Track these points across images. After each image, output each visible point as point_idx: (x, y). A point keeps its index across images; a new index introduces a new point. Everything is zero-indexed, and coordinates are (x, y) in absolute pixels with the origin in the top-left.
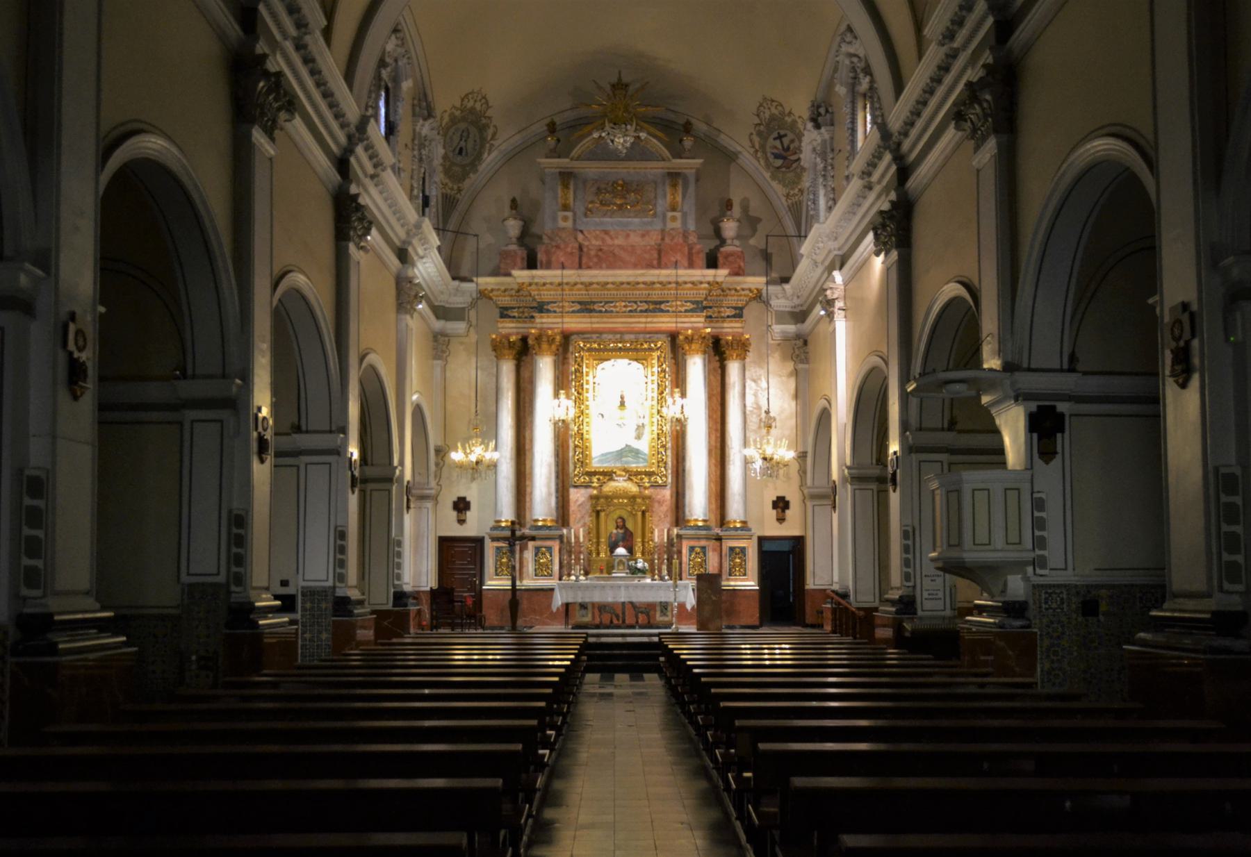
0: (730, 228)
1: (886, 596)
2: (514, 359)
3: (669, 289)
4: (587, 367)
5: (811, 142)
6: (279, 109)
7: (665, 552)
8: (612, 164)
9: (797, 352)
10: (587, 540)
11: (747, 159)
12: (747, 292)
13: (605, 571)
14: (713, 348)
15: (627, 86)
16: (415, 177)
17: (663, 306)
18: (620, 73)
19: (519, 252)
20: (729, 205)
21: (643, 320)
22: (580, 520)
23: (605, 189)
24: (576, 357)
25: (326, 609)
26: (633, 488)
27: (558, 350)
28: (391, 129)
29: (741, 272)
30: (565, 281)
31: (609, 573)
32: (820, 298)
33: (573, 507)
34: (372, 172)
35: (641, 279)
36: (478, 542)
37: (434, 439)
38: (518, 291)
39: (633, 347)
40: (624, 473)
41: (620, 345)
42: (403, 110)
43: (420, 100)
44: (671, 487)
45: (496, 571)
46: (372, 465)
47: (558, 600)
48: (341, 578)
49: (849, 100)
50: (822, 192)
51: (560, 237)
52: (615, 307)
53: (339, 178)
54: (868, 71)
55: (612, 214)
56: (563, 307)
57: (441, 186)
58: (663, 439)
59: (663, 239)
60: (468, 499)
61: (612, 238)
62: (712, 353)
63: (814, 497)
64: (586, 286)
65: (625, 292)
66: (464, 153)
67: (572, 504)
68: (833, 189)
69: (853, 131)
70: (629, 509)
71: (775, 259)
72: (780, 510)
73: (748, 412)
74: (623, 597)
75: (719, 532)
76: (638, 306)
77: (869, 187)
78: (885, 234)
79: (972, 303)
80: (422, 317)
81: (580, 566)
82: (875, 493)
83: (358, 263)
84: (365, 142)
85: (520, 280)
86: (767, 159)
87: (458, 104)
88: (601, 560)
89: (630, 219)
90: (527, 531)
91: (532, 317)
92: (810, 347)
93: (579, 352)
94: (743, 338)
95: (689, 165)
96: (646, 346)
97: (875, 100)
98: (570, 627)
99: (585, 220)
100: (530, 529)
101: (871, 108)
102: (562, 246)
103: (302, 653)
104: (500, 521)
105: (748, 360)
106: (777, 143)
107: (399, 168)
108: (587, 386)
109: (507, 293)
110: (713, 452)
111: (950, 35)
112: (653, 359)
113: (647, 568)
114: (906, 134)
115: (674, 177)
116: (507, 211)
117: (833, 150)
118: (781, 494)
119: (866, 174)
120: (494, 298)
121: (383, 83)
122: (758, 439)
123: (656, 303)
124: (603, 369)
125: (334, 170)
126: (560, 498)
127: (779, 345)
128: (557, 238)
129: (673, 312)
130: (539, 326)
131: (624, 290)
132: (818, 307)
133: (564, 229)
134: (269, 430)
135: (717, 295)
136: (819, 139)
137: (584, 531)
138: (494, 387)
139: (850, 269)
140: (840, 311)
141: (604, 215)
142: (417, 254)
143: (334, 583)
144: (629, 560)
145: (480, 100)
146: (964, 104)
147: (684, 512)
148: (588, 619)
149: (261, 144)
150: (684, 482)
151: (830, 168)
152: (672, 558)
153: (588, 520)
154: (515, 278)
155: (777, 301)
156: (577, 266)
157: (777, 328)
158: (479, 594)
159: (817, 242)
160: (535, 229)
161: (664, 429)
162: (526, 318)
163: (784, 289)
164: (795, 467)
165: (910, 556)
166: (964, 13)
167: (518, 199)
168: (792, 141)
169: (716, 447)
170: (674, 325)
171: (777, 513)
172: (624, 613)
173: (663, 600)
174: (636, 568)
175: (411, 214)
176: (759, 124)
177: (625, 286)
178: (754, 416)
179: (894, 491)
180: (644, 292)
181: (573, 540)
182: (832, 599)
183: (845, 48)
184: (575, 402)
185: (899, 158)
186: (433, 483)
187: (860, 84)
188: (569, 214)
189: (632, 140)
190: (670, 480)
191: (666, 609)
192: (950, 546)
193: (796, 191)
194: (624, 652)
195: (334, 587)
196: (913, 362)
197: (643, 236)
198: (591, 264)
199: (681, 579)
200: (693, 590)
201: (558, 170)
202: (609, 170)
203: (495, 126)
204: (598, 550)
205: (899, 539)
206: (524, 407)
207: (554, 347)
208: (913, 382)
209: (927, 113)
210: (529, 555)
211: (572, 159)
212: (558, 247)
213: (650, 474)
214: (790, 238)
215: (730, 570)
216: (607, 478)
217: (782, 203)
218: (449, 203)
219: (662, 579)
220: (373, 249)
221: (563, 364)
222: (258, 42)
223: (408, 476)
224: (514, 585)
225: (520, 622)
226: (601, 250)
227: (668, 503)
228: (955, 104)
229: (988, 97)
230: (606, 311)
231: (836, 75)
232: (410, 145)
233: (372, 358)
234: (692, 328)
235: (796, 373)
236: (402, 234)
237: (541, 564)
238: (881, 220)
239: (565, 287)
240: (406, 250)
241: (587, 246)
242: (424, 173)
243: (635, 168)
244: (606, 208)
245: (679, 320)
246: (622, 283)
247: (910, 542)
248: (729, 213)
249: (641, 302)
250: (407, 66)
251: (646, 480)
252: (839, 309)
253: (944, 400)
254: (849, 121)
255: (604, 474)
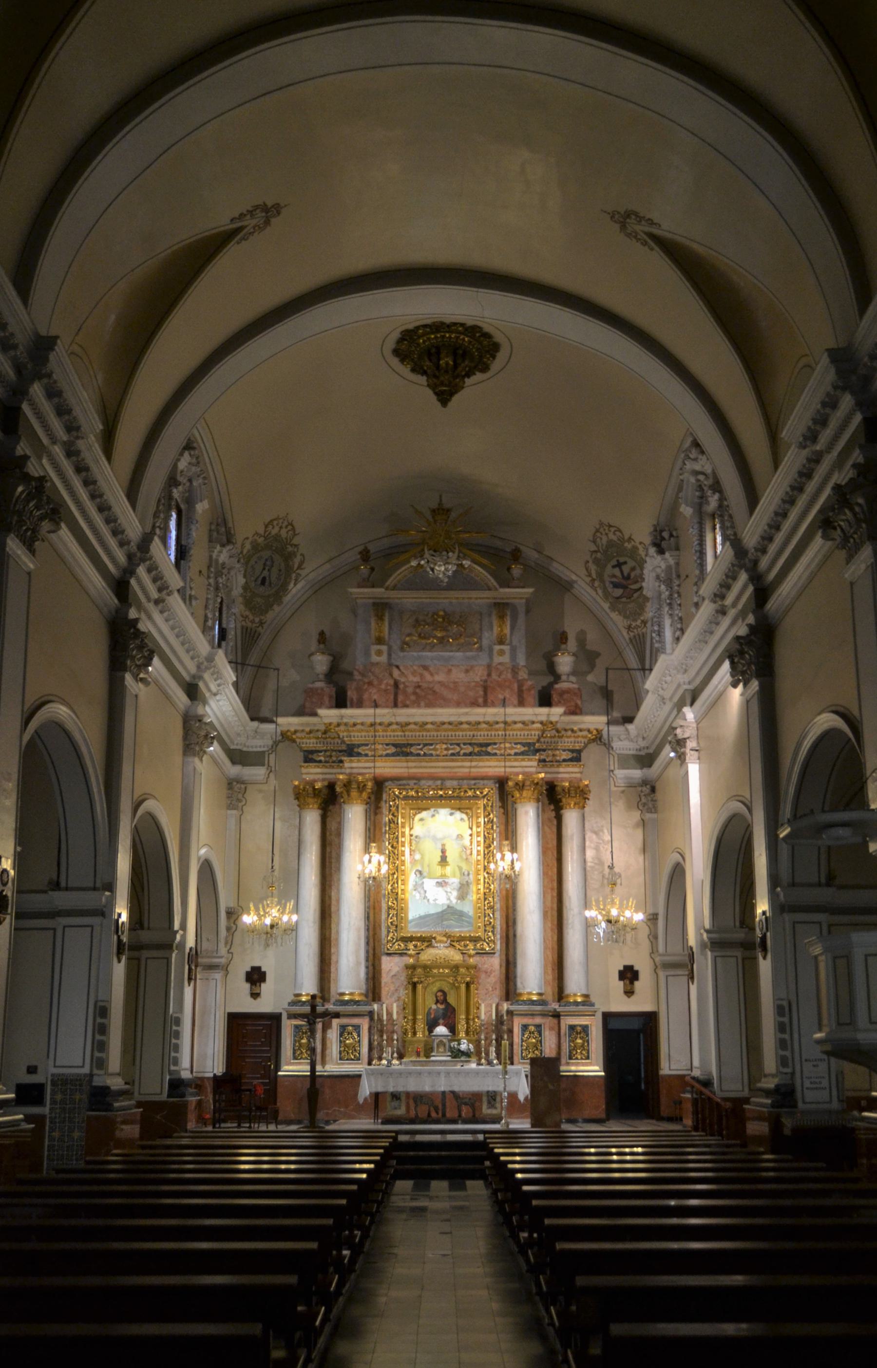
0: (565, 662)
1: (759, 1085)
2: (319, 808)
3: (497, 730)
4: (402, 817)
5: (653, 570)
6: (42, 518)
7: (493, 1031)
8: (434, 594)
9: (644, 800)
10: (401, 1016)
11: (584, 589)
12: (585, 733)
13: (422, 1054)
14: (547, 796)
15: (448, 510)
16: (210, 607)
17: (489, 749)
18: (441, 496)
19: (327, 690)
20: (563, 638)
21: (468, 764)
22: (393, 994)
23: (424, 621)
24: (390, 806)
25: (80, 1100)
26: (456, 957)
27: (369, 798)
28: (182, 552)
29: (578, 711)
30: (378, 720)
31: (428, 1056)
32: (669, 738)
33: (385, 979)
34: (156, 597)
35: (464, 719)
36: (274, 1019)
37: (225, 900)
38: (325, 732)
39: (455, 794)
40: (445, 939)
41: (441, 793)
42: (198, 534)
43: (218, 525)
44: (500, 955)
45: (294, 1053)
46: (149, 929)
47: (366, 1090)
48: (100, 1064)
49: (695, 520)
50: (667, 622)
51: (373, 673)
52: (435, 749)
53: (116, 601)
54: (717, 487)
55: (432, 647)
56: (375, 750)
57: (241, 619)
58: (491, 899)
59: (489, 675)
60: (263, 969)
61: (432, 675)
62: (546, 801)
63: (667, 966)
64: (402, 726)
65: (446, 734)
66: (267, 584)
67: (384, 975)
68: (681, 619)
69: (702, 554)
70: (451, 980)
71: (616, 697)
72: (628, 982)
73: (588, 869)
74: (442, 1085)
75: (557, 1007)
76: (461, 749)
77: (723, 612)
78: (743, 662)
79: (851, 735)
80: (214, 760)
81: (392, 1047)
82: (740, 961)
83: (136, 696)
84: (148, 563)
85: (327, 721)
86: (605, 590)
87: (261, 531)
88: (419, 1041)
89: (451, 654)
90: (330, 1007)
91: (341, 761)
92: (659, 795)
93: (394, 800)
94: (581, 785)
95: (519, 594)
96: (470, 793)
97: (726, 518)
98: (380, 1121)
99: (402, 654)
100: (334, 1004)
101: (723, 528)
102: (375, 682)
103: (49, 1156)
104: (300, 995)
105: (587, 809)
106: (617, 572)
107: (190, 596)
108: (403, 839)
109: (311, 735)
110: (549, 914)
111: (811, 437)
112: (479, 808)
113: (472, 1050)
114: (764, 551)
115: (501, 608)
116: (314, 645)
117: (679, 576)
118: (628, 963)
119: (719, 596)
120: (298, 741)
121: (173, 503)
122: (601, 899)
123: (481, 745)
124: (421, 820)
125: (109, 591)
126: (371, 968)
127: (623, 792)
128: (370, 674)
129: (501, 755)
130: (348, 771)
131: (446, 730)
132: (668, 747)
133: (377, 663)
134: (10, 884)
135: (551, 737)
136: (663, 565)
137: (397, 1006)
138: (296, 840)
139: (703, 704)
140: (692, 752)
141: (423, 649)
142: (209, 690)
143: (91, 1070)
144: (450, 1041)
145: (286, 527)
146: (833, 509)
147: (515, 985)
148: (401, 1112)
149: (19, 556)
150: (515, 948)
151: (676, 595)
152: (502, 1038)
153: (404, 994)
154: (321, 717)
155: (620, 743)
156: (393, 704)
157: (621, 774)
158: (273, 1081)
159: (664, 675)
160: (345, 665)
161: (492, 887)
162: (334, 762)
163: (627, 730)
164: (644, 932)
165: (786, 1036)
166: (828, 410)
167: (328, 634)
168: (633, 569)
169: (552, 908)
170: (503, 770)
171: (625, 984)
172: (444, 1105)
173: (491, 1089)
174: (459, 1050)
175: (203, 646)
176: (595, 552)
177: (446, 726)
178: (596, 873)
179: (765, 958)
180: (468, 733)
181: (385, 1017)
182: (693, 1087)
183: (689, 465)
184: (389, 856)
185: (756, 578)
186: (223, 950)
187: (708, 503)
188: (384, 648)
189: (455, 568)
190: (498, 947)
191: (495, 1100)
192: (839, 1024)
193: (639, 622)
194: (443, 1153)
195: (91, 1075)
196: (782, 805)
197: (467, 671)
198: (408, 702)
199: (512, 1063)
200: (527, 1076)
201: (371, 601)
202: (428, 600)
203: (302, 555)
204: (414, 1028)
205: (772, 1015)
206: (331, 862)
207: (365, 795)
208: (786, 826)
209: (787, 526)
210: (333, 1035)
211: (387, 589)
212: (370, 683)
213: (475, 940)
214: (631, 672)
215: (570, 1052)
216: (426, 944)
217: (623, 636)
218: (249, 637)
219: (490, 1063)
220: (156, 682)
221: (376, 814)
222: (18, 443)
223: (191, 942)
224: (313, 1070)
225: (320, 1115)
226: (419, 687)
227: (497, 973)
228: (820, 511)
229: (861, 501)
230: (425, 755)
231: (680, 495)
232: (205, 571)
233: (150, 805)
234: (523, 774)
235: (643, 823)
236: (193, 669)
237: (346, 1045)
238: (738, 647)
239: (378, 727)
240: (197, 685)
241: (404, 683)
242: (221, 603)
243: (457, 598)
244: (424, 641)
245: (508, 764)
246: (443, 723)
247: (786, 1020)
248: (563, 646)
249: (465, 744)
250: (203, 487)
251: (471, 946)
252: (692, 750)
253: (819, 848)
254: (696, 543)
255: (422, 939)
